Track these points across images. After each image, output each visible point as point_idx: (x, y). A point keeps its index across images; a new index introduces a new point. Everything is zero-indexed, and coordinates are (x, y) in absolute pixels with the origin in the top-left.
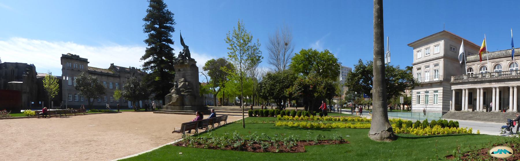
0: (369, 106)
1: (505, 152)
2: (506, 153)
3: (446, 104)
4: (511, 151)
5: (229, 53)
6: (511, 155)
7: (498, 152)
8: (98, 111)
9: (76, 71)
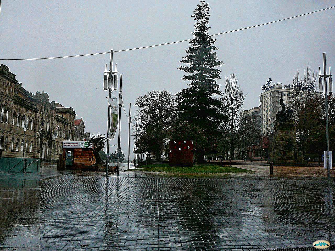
1: (324, 244)
2: (325, 246)
9: (202, 27)
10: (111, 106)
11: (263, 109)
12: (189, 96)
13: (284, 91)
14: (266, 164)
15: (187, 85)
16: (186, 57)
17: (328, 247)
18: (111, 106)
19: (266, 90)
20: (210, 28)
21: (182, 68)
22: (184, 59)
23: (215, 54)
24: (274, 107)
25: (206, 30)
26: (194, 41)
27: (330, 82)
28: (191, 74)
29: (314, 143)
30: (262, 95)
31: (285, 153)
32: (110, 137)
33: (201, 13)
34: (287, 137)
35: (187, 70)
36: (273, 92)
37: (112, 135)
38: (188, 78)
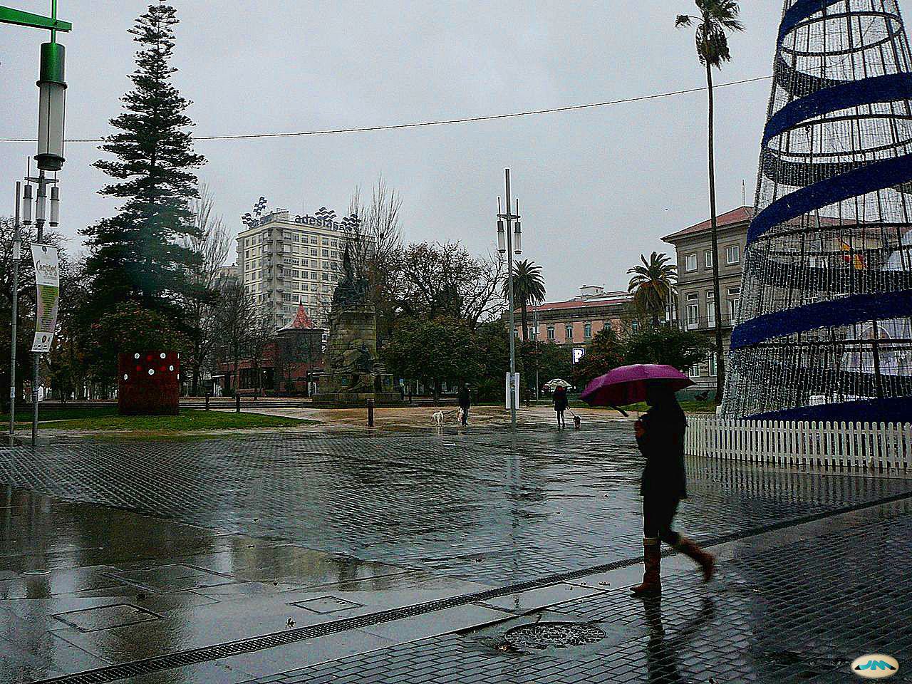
1: (882, 665)
2: (884, 669)
3: (654, 617)
9: (154, 63)
10: (39, 266)
11: (243, 270)
12: (117, 236)
13: (294, 231)
14: (311, 403)
15: (115, 207)
16: (109, 137)
17: (893, 672)
18: (39, 266)
19: (253, 224)
20: (176, 70)
21: (101, 165)
22: (106, 141)
23: (183, 137)
24: (270, 268)
25: (166, 73)
26: (135, 98)
28: (123, 182)
29: (403, 354)
30: (241, 236)
31: (356, 378)
32: (39, 346)
33: (155, 30)
34: (360, 342)
35: (115, 170)
36: (270, 230)
37: (43, 342)
38: (120, 191)
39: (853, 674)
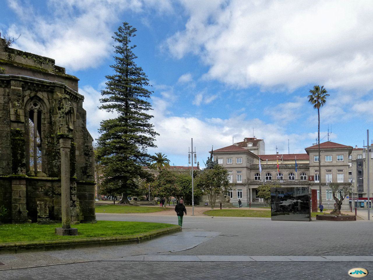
0: (135, 142)
2: (361, 274)
4: (366, 272)
5: (115, 65)
6: (365, 275)
7: (355, 272)
8: (157, 211)
27: (195, 157)
39: (348, 275)
